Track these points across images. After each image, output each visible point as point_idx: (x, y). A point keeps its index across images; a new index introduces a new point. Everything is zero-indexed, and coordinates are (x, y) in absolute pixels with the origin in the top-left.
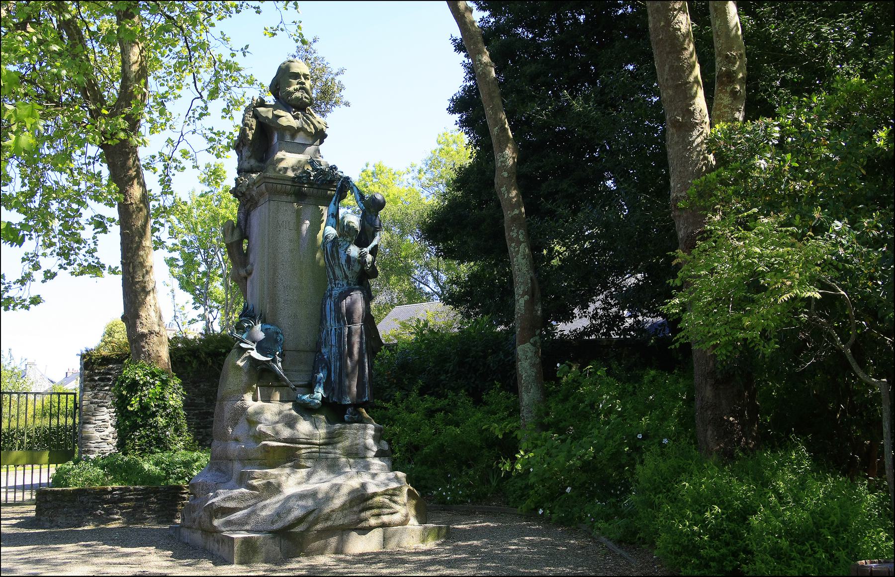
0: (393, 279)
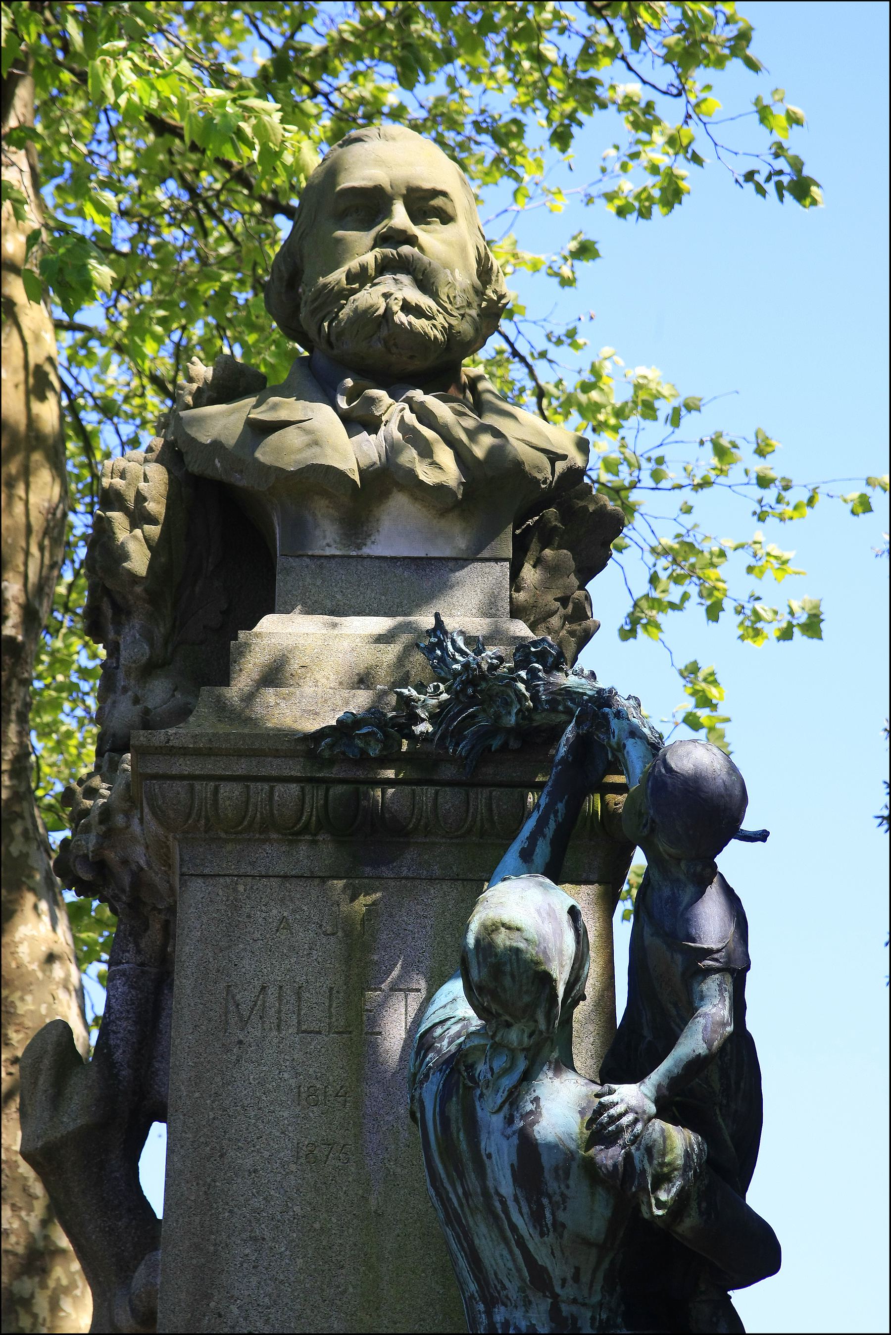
0: (114, 1260)
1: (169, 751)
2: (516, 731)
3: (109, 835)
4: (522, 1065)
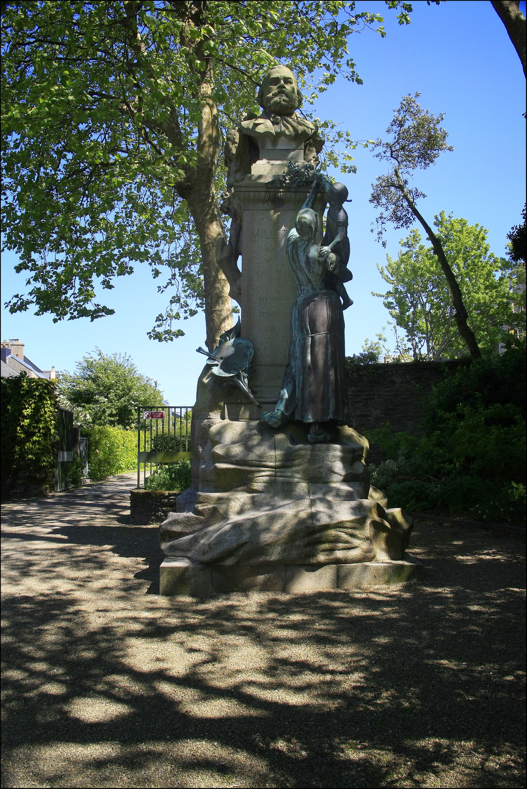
1: (241, 187)
2: (305, 182)
3: (230, 203)
4: (306, 243)
